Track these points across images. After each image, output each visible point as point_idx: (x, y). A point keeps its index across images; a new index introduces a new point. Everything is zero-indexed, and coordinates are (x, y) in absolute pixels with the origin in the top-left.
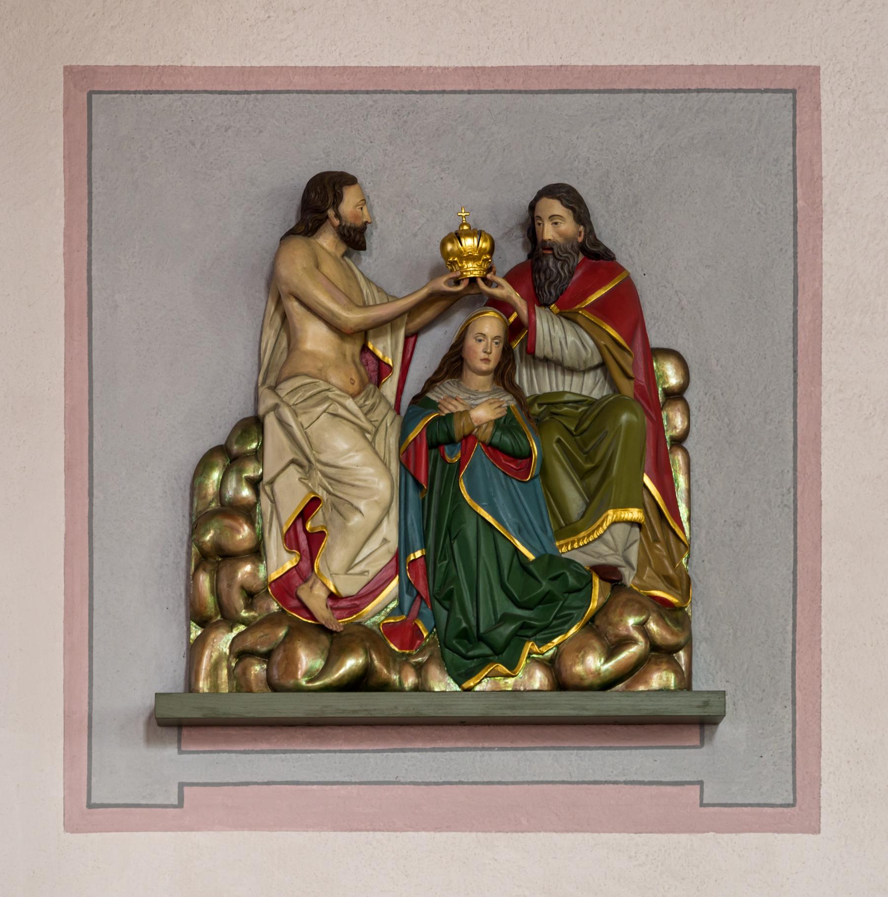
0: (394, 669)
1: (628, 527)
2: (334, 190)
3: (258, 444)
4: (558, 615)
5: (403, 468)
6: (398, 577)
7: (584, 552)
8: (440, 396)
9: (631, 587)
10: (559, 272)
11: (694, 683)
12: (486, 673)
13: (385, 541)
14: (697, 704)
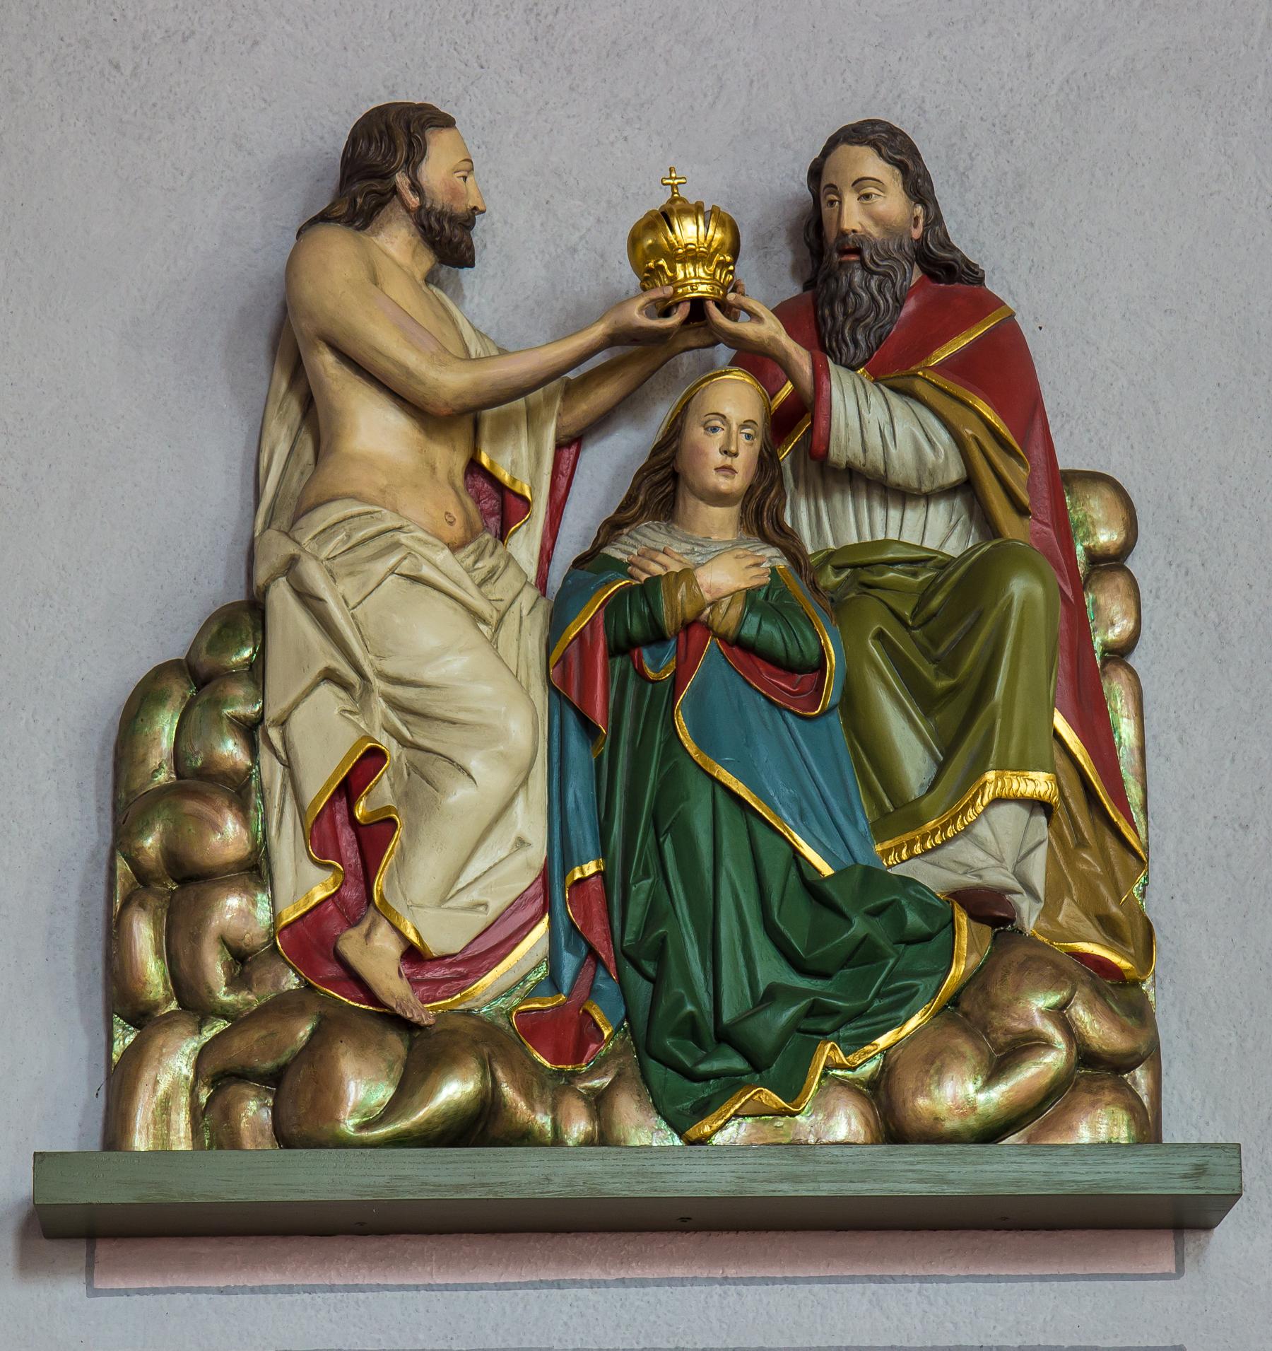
0: (542, 1102)
1: (1020, 812)
2: (410, 135)
3: (254, 649)
4: (883, 989)
5: (555, 697)
6: (547, 918)
7: (933, 864)
8: (630, 549)
9: (1032, 937)
10: (873, 298)
11: (1164, 1136)
12: (737, 1106)
13: (521, 843)
14: (1180, 1170)
